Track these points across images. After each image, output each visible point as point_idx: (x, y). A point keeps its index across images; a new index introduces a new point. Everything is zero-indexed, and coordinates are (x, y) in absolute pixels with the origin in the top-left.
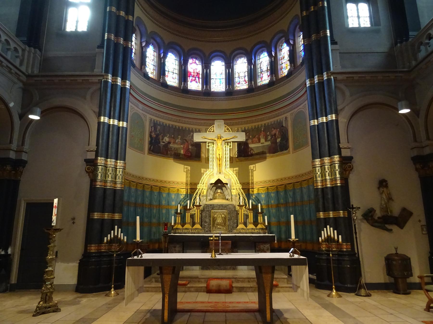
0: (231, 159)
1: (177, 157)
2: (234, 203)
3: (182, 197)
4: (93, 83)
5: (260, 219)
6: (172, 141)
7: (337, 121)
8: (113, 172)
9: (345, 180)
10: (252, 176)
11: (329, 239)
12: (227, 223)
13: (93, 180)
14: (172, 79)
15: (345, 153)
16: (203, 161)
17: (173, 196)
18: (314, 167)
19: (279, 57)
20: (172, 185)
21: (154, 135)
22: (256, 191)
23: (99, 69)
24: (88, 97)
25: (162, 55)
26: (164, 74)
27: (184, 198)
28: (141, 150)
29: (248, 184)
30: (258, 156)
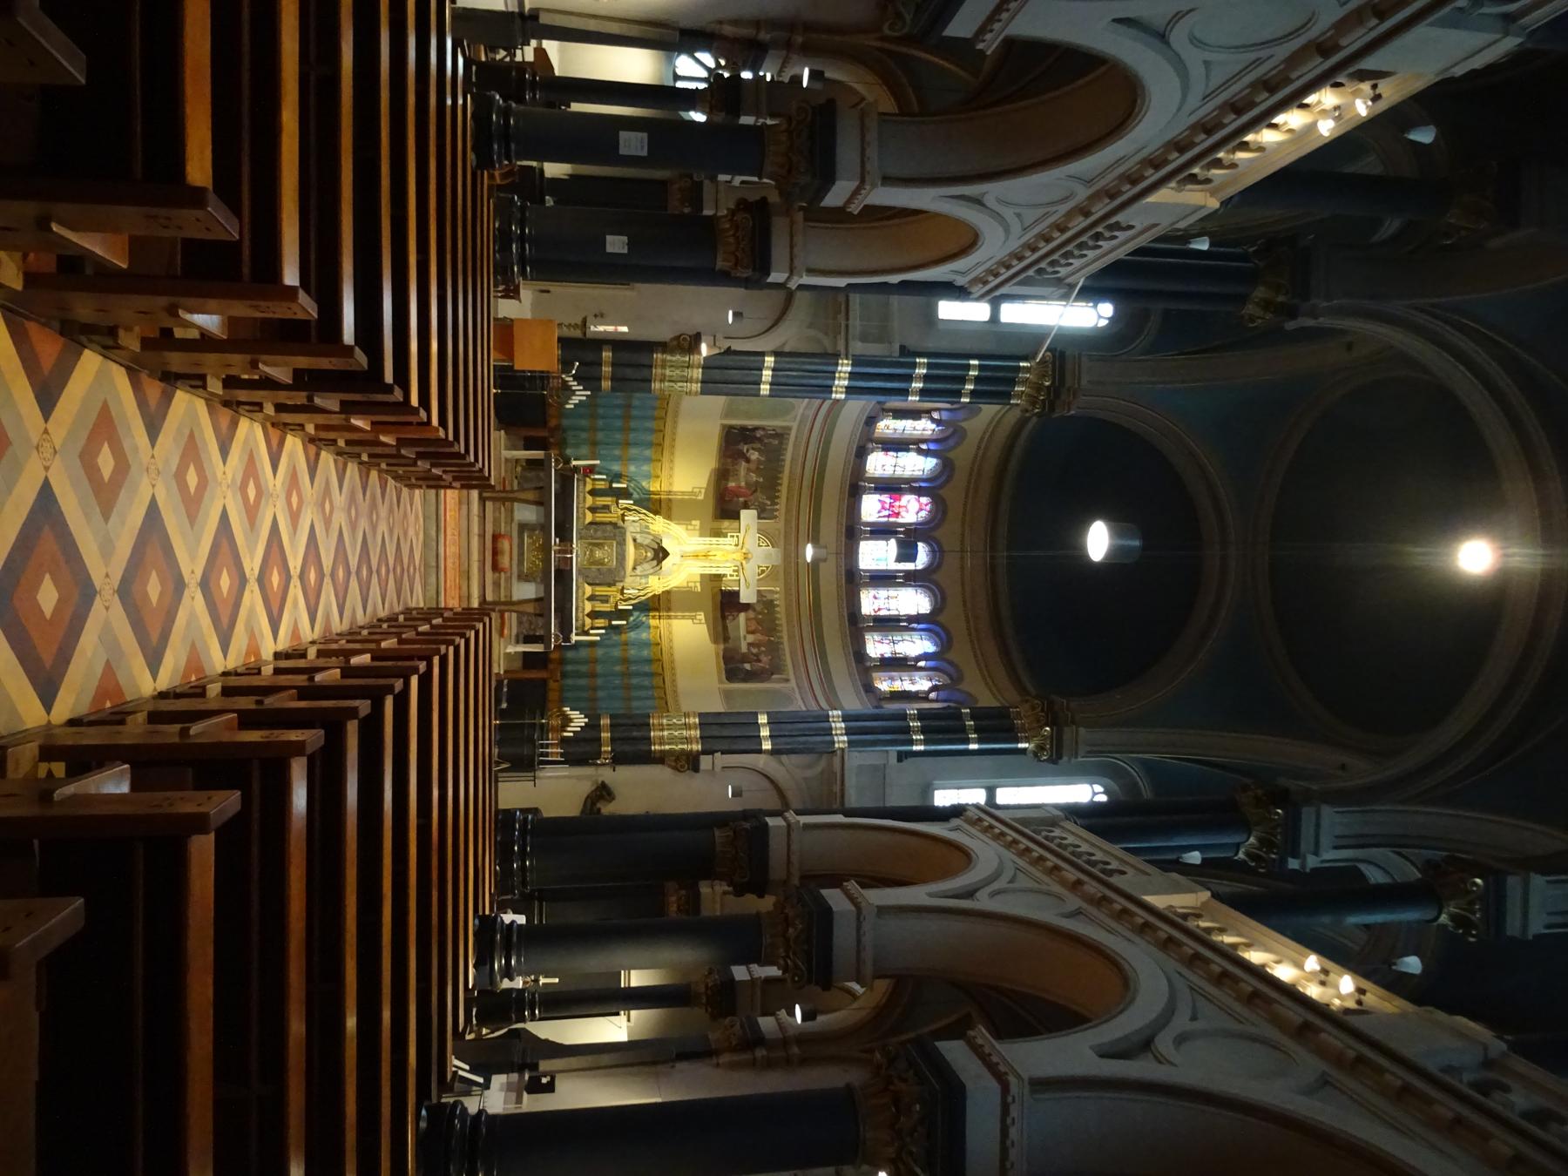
0: (719, 577)
1: (721, 476)
2: (628, 580)
3: (644, 484)
4: (835, 344)
5: (601, 622)
6: (753, 466)
7: (760, 751)
8: (680, 379)
9: (660, 759)
10: (683, 617)
11: (567, 721)
12: (594, 567)
13: (663, 347)
14: (879, 464)
15: (705, 761)
16: (716, 524)
17: (645, 468)
18: (686, 715)
19: (917, 675)
20: (666, 465)
21: (759, 434)
22: (653, 622)
23: (858, 347)
24: (812, 332)
25: (924, 447)
26: (886, 450)
27: (642, 489)
28: (727, 415)
29: (669, 609)
30: (720, 628)
